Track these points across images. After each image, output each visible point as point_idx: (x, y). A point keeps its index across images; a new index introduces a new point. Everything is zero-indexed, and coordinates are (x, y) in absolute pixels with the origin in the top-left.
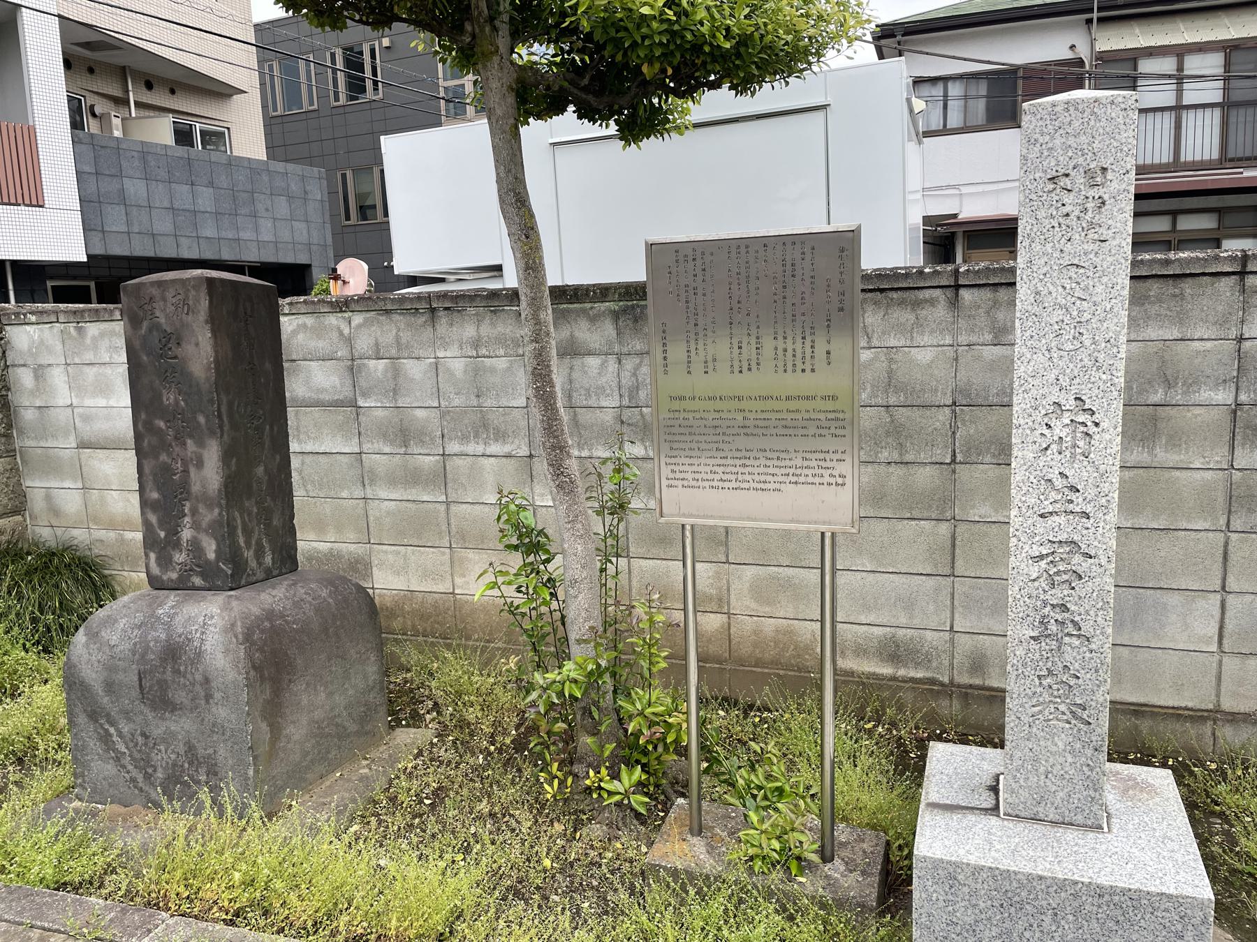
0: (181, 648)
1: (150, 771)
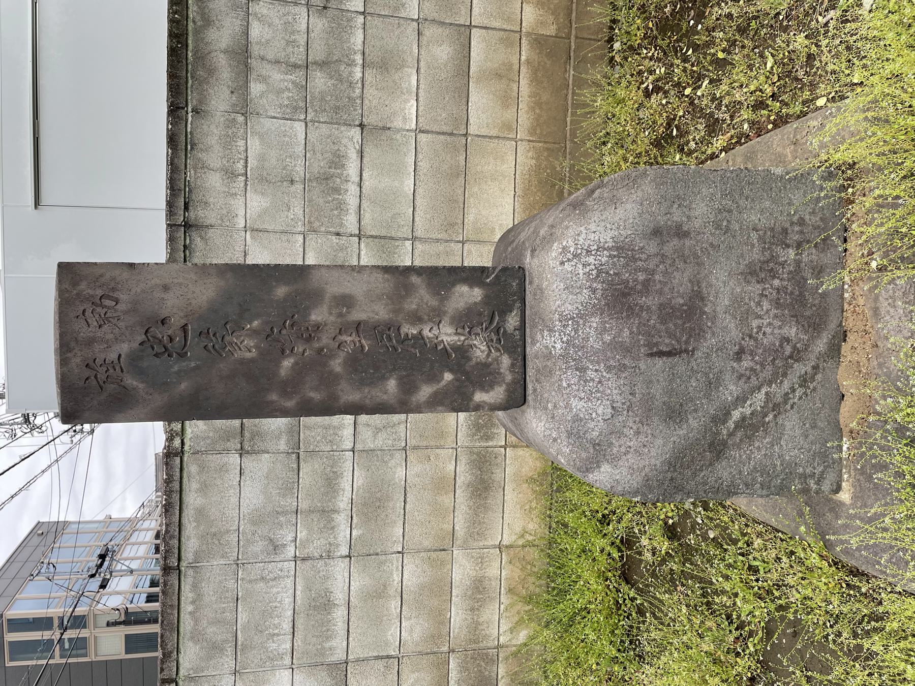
0: (611, 284)
1: (788, 350)
